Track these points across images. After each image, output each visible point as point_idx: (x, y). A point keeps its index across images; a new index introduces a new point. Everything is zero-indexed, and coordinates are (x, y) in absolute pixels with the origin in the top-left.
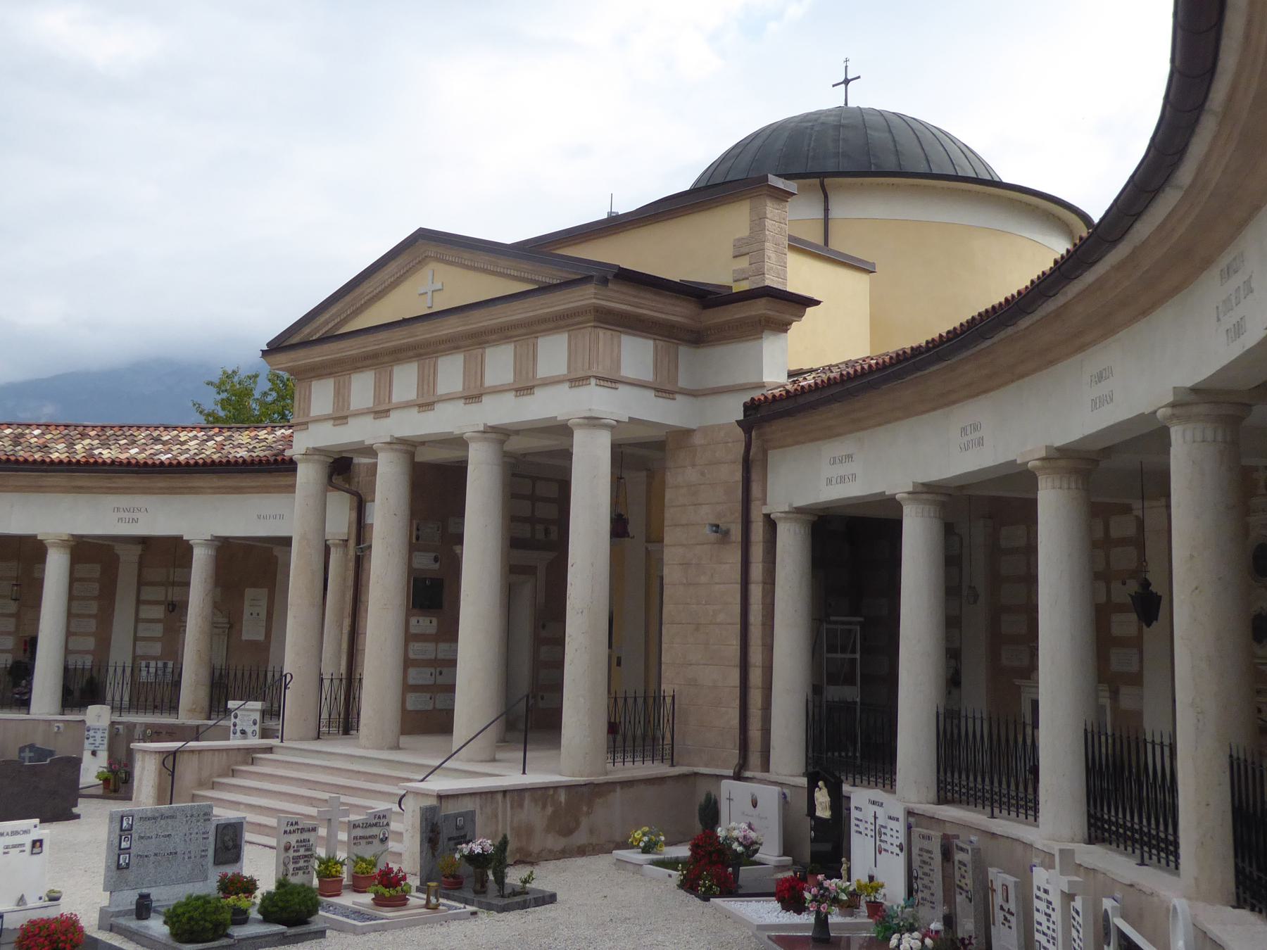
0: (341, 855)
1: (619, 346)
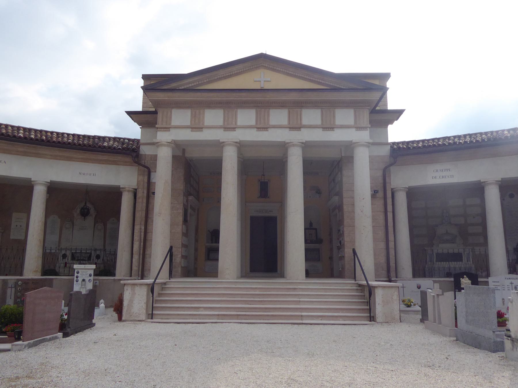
0: (462, 266)
1: (334, 117)
